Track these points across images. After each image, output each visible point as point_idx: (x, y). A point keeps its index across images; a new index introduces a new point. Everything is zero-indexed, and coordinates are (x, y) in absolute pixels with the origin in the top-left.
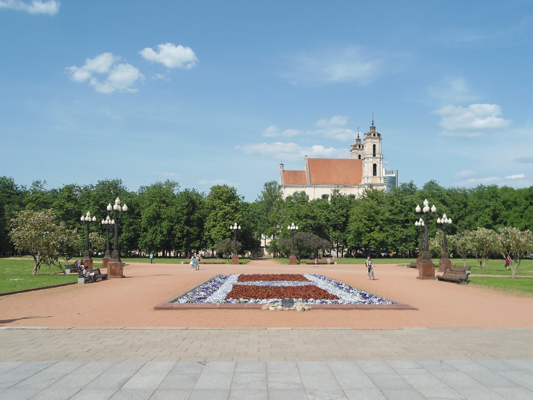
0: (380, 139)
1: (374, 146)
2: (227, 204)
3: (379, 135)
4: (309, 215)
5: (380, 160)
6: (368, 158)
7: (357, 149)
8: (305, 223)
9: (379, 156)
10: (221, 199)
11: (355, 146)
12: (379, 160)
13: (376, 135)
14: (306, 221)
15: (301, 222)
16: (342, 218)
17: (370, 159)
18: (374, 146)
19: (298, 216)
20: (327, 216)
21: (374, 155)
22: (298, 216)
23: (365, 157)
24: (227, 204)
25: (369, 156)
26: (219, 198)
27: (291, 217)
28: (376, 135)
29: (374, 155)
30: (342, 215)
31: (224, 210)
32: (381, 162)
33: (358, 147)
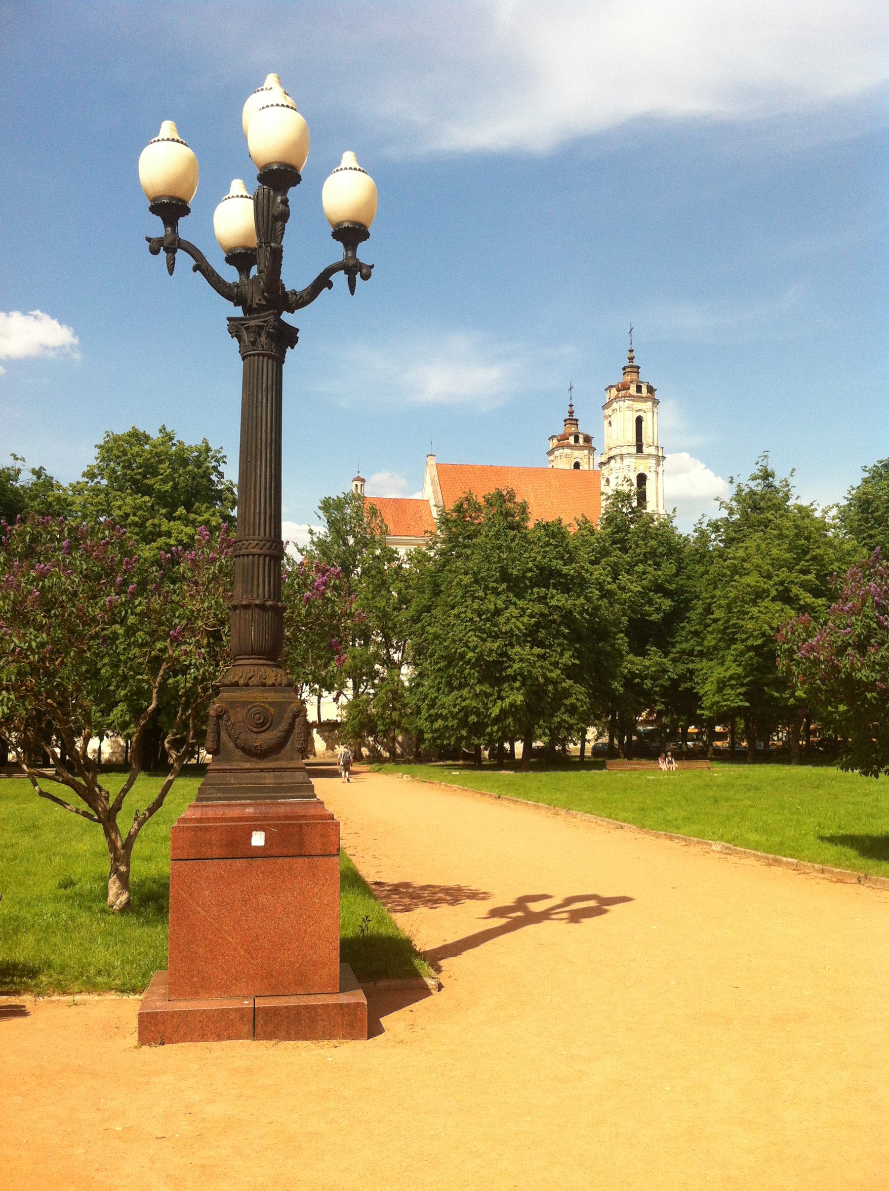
0: (592, 450)
1: (639, 421)
2: (181, 511)
3: (588, 439)
4: (559, 574)
5: (658, 465)
6: (622, 456)
7: (569, 446)
8: (538, 608)
9: (652, 450)
10: (147, 491)
11: (564, 437)
12: (652, 462)
13: (644, 389)
14: (542, 599)
15: (520, 603)
16: (657, 598)
17: (627, 461)
18: (639, 421)
19: (505, 576)
20: (799, 523)
21: (639, 448)
22: (505, 576)
23: (612, 453)
24: (181, 511)
25: (624, 451)
26: (142, 489)
27: (476, 582)
28: (644, 389)
29: (639, 448)
30: (659, 588)
31: (162, 541)
32: (660, 469)
33: (571, 440)
